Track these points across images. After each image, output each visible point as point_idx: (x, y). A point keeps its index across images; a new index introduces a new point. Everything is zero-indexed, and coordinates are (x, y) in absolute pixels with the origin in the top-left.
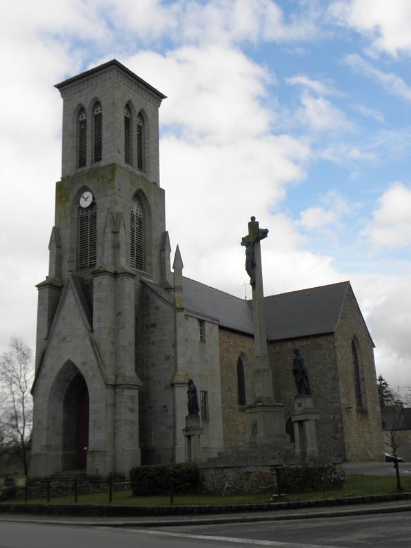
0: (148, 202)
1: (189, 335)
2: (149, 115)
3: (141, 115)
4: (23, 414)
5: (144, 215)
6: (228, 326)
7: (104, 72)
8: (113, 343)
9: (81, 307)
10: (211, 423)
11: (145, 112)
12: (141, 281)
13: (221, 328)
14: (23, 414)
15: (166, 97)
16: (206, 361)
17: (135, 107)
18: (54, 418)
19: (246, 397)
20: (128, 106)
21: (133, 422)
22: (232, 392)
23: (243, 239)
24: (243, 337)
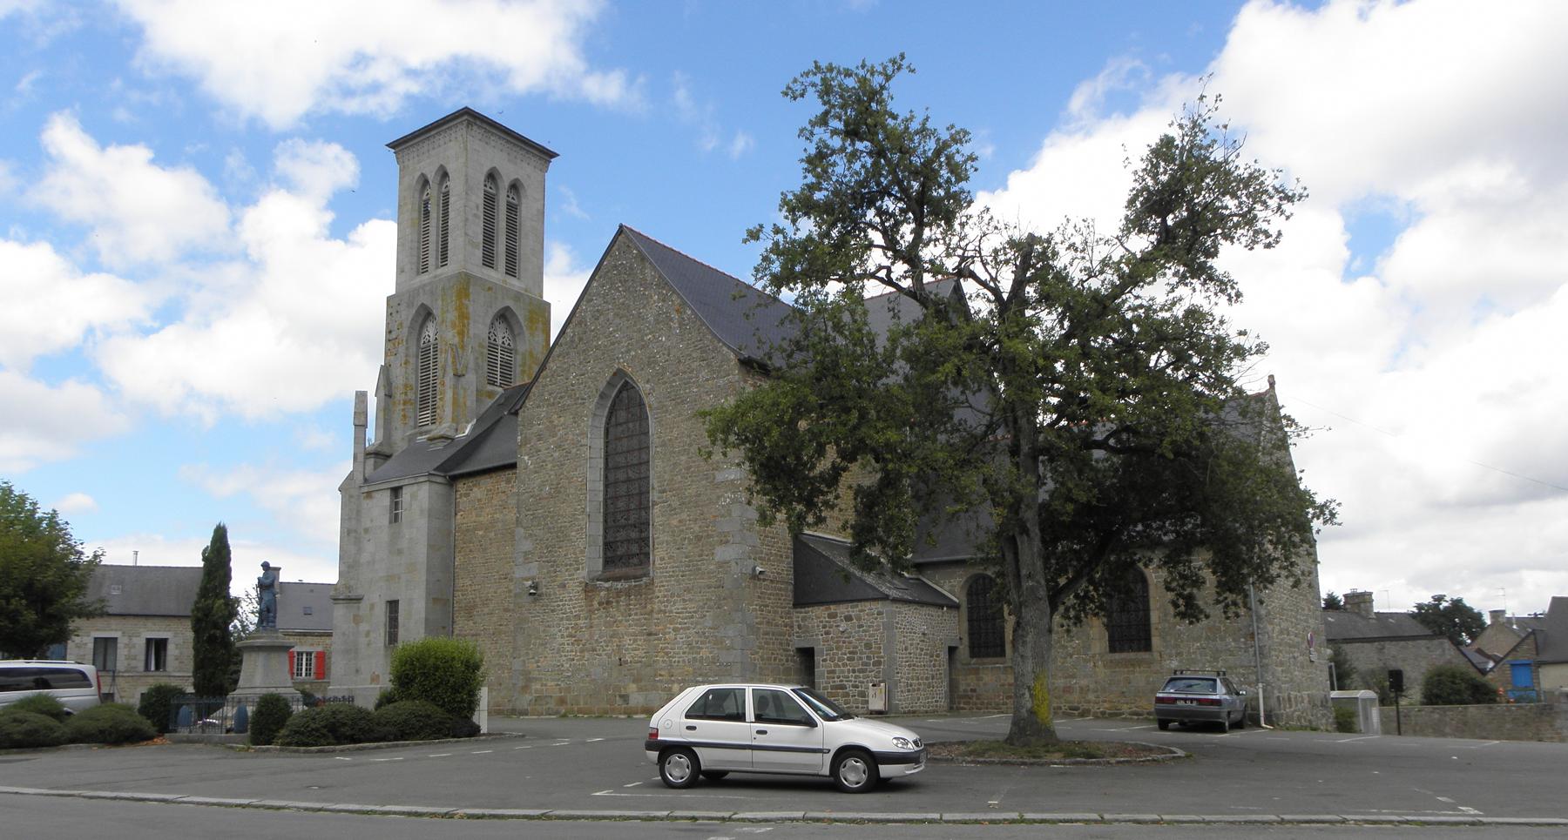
16: (400, 552)
23: (1005, 188)
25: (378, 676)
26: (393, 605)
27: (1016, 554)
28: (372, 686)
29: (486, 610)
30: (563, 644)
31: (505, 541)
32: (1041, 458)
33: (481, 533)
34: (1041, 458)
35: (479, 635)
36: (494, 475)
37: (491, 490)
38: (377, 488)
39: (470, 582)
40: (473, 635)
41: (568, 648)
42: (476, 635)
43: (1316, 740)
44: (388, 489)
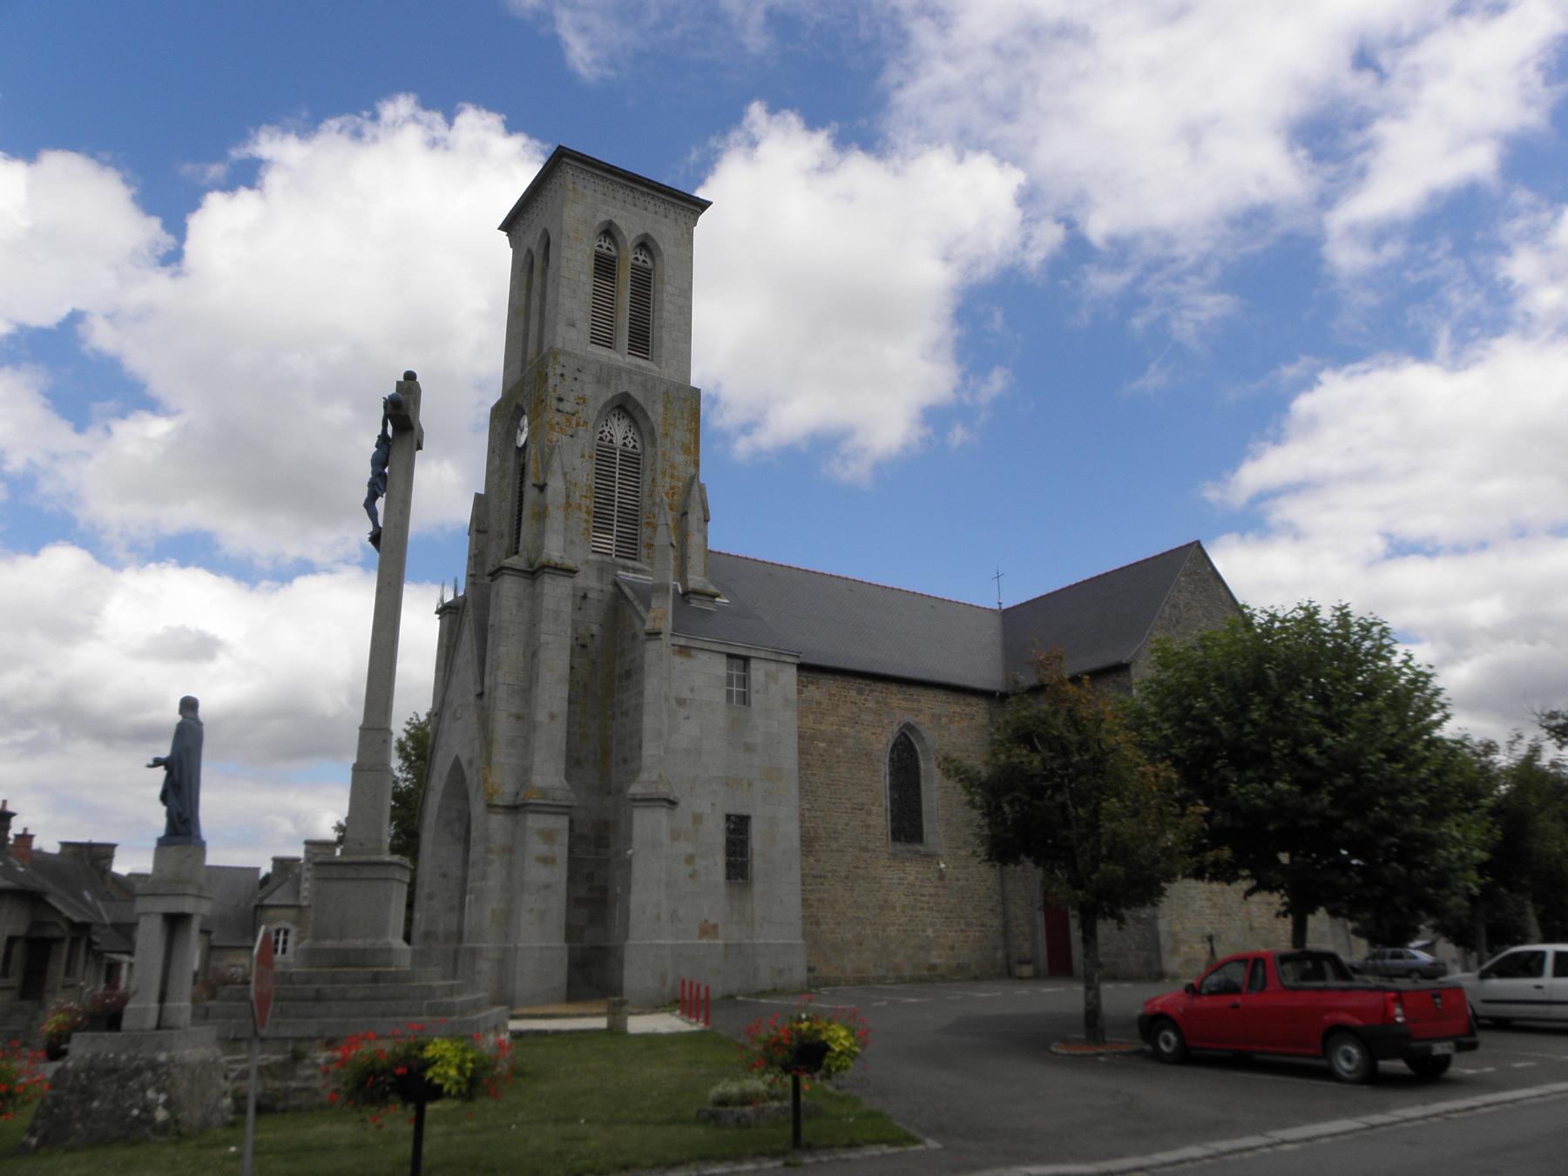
0: (647, 418)
1: (692, 690)
2: (666, 247)
3: (645, 244)
4: (952, 848)
5: (643, 445)
6: (823, 662)
7: (669, 202)
8: (519, 717)
9: (475, 642)
10: (758, 886)
11: (652, 240)
12: (615, 584)
13: (802, 667)
14: (952, 848)
15: (710, 203)
16: (749, 748)
17: (625, 233)
18: (444, 875)
19: (925, 824)
20: (609, 231)
21: (547, 887)
22: (869, 813)
23: (73, 310)
24: (912, 690)
25: (715, 927)
26: (738, 828)
27: (531, 804)
28: (704, 941)
29: (834, 846)
30: (1202, 907)
31: (859, 763)
32: (1204, 778)
33: (822, 745)
34: (1204, 778)
35: (824, 877)
36: (838, 677)
37: (834, 695)
38: (706, 646)
39: (809, 806)
40: (815, 877)
41: (1208, 911)
42: (820, 877)
43: (1063, 989)
44: (793, 663)
